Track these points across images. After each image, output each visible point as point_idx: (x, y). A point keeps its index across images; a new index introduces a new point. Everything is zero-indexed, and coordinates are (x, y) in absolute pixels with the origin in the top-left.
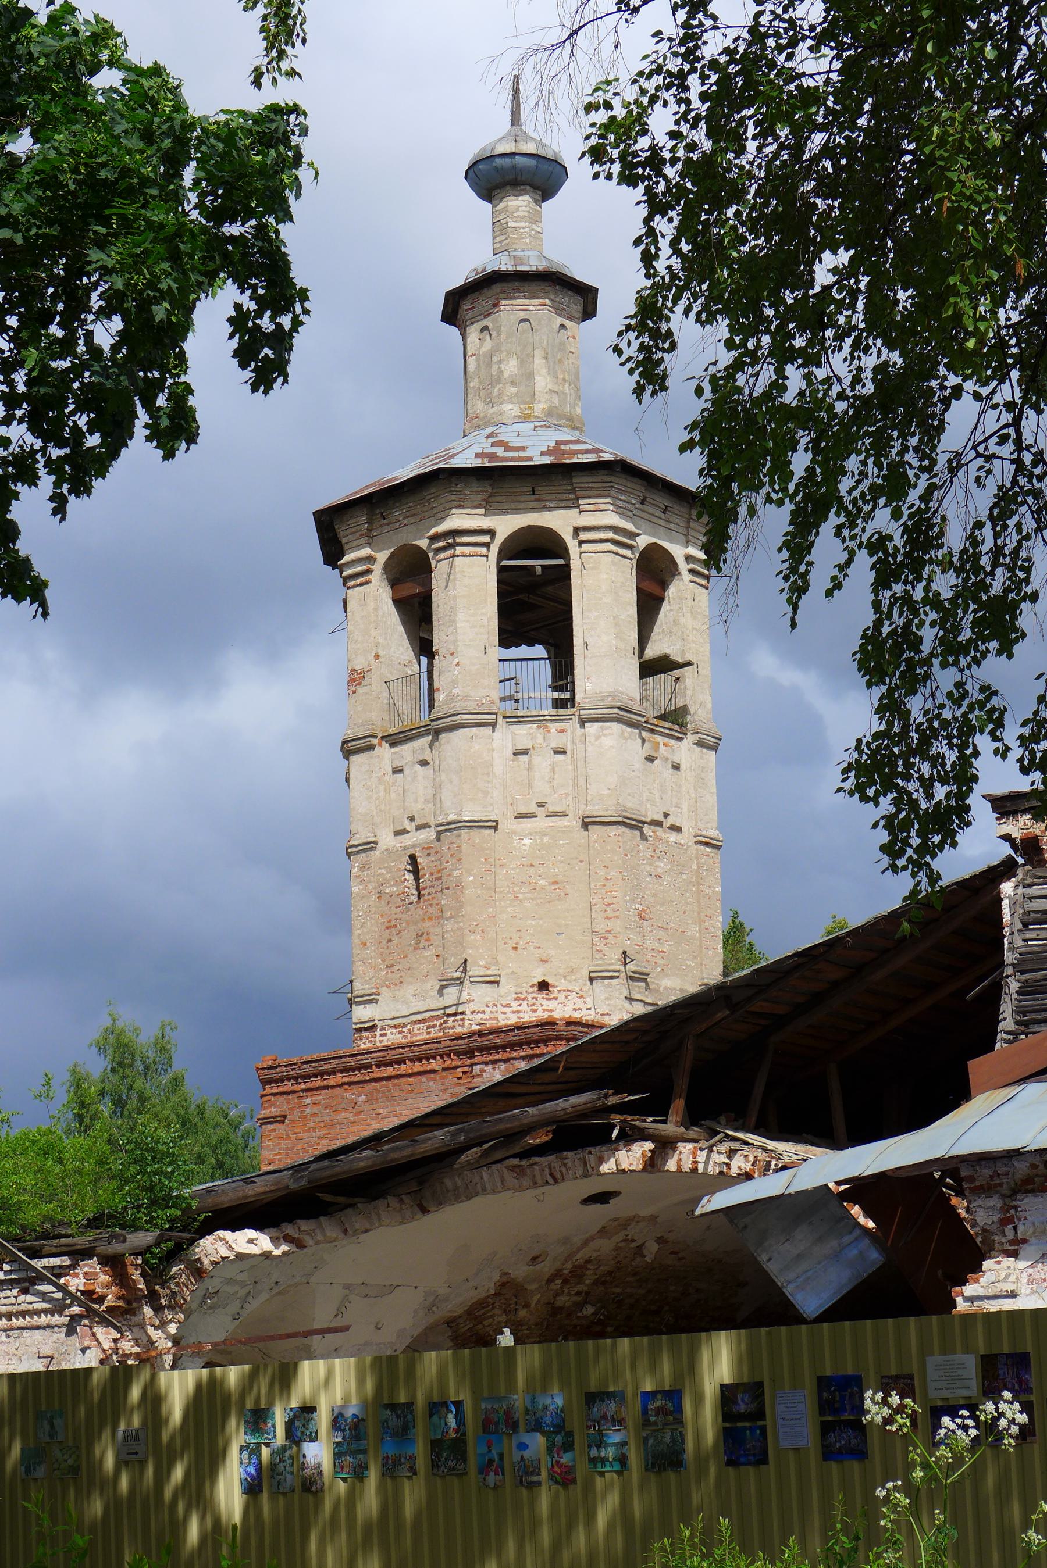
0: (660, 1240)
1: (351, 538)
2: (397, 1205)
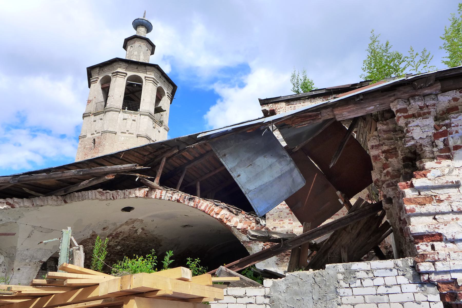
0: (143, 229)
1: (94, 74)
2: (56, 199)
